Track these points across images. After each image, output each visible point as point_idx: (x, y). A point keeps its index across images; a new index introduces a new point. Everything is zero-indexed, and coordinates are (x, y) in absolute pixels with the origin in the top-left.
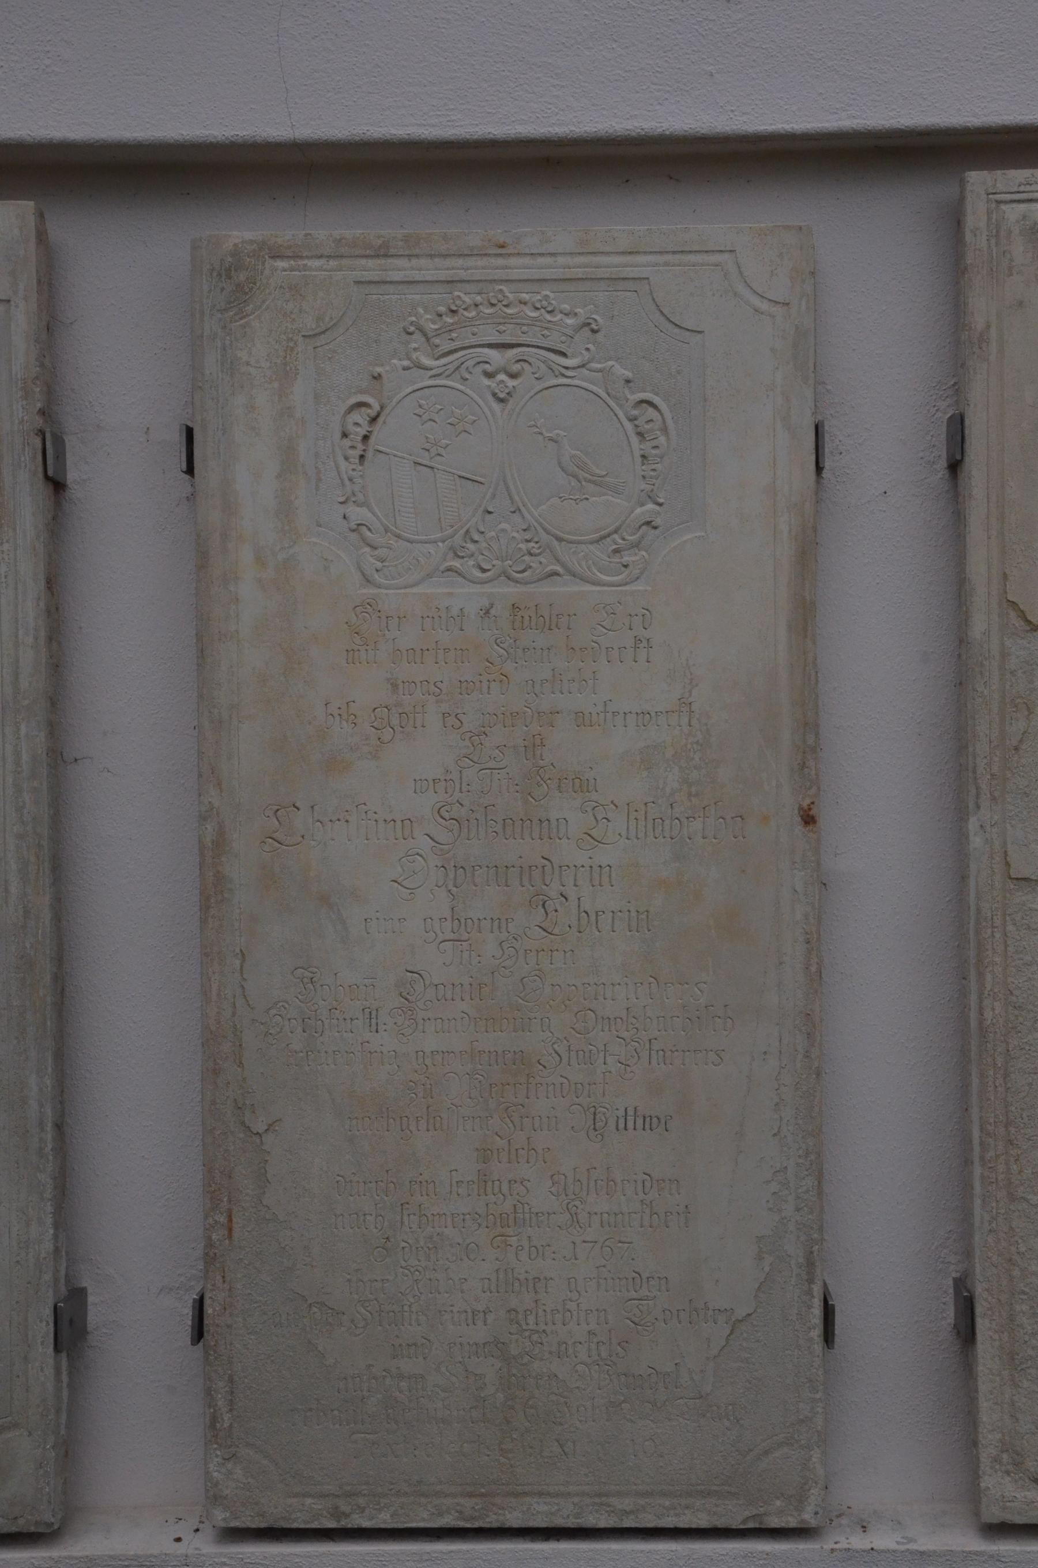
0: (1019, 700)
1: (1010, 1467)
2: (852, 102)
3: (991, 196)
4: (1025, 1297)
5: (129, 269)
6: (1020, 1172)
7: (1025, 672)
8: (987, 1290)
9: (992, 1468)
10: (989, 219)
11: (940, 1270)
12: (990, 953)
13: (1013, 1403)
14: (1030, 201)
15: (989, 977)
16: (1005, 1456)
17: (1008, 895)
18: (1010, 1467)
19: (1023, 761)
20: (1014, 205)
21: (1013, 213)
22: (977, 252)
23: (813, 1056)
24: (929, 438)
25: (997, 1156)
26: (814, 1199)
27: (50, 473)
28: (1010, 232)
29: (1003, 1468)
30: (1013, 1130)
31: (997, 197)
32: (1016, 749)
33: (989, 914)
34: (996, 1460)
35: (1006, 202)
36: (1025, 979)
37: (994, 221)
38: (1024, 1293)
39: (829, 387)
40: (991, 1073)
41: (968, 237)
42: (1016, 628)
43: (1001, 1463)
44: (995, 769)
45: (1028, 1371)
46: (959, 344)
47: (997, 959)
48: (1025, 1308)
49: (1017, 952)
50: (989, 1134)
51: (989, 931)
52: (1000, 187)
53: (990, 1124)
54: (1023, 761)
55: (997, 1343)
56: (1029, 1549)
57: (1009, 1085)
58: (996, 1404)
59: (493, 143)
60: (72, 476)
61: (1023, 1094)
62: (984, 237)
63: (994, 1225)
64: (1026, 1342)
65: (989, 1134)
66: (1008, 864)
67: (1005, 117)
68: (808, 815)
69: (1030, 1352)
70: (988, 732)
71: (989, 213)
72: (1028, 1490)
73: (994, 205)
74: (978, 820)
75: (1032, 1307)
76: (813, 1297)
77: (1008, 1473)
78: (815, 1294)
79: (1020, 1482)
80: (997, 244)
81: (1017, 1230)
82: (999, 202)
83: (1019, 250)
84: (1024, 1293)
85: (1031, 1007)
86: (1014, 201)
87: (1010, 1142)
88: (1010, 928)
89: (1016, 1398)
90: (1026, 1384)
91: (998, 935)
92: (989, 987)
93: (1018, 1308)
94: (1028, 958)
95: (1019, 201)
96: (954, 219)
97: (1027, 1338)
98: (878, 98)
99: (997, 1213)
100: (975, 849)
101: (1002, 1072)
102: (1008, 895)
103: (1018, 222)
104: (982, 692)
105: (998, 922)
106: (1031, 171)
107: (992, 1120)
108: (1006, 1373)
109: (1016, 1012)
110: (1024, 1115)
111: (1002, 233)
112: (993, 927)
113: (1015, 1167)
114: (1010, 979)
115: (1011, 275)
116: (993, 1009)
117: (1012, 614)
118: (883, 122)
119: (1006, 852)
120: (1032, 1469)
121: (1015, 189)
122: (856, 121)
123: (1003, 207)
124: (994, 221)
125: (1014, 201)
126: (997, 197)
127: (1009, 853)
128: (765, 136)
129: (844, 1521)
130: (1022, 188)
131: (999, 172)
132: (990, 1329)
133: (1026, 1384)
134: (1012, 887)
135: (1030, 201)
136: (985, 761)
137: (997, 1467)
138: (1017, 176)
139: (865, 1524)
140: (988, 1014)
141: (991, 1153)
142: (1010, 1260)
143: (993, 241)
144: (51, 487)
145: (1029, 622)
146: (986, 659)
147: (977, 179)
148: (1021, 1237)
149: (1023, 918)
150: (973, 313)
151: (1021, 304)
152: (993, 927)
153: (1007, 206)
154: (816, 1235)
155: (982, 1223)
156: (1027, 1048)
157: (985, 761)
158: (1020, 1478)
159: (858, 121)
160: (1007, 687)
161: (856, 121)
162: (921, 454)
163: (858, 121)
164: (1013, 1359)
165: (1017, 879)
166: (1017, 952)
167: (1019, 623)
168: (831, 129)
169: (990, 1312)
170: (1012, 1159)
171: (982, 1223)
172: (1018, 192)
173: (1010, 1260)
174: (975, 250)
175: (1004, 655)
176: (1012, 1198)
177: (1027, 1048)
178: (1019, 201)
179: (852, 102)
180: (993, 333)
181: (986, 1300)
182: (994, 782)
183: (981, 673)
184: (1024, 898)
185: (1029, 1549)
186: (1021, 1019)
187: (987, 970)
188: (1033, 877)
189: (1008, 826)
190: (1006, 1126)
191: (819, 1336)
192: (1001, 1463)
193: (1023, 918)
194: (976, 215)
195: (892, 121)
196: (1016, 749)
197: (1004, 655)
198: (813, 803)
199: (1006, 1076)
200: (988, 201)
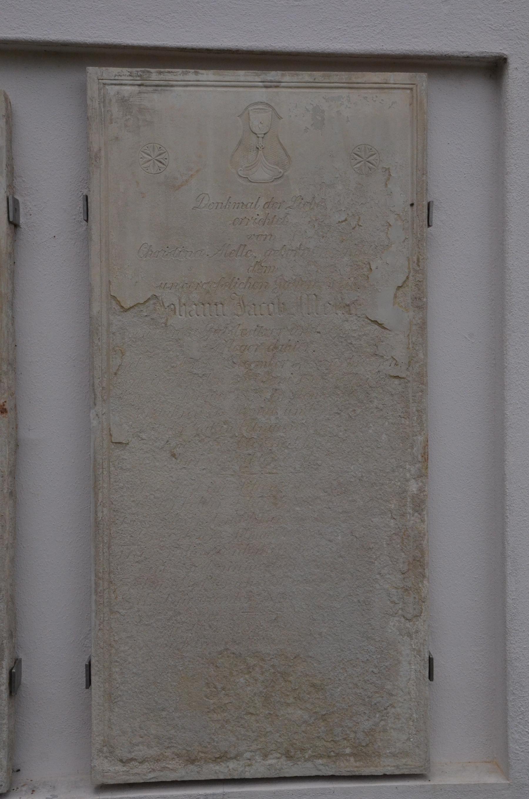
0: (117, 348)
1: (108, 755)
2: (23, 24)
3: (100, 81)
4: (117, 664)
5: (40, 106)
6: (116, 598)
7: (120, 334)
8: (97, 661)
9: (98, 755)
10: (100, 93)
11: (84, 651)
12: (101, 482)
13: (110, 720)
14: (121, 84)
15: (100, 495)
16: (105, 749)
17: (111, 451)
18: (108, 755)
19: (119, 380)
20: (113, 86)
21: (112, 90)
22: (93, 110)
23: (5, 538)
24: (78, 208)
25: (104, 590)
26: (4, 615)
27: (11, 220)
28: (111, 100)
29: (104, 755)
30: (112, 576)
31: (104, 81)
32: (115, 374)
33: (101, 461)
34: (101, 751)
35: (108, 85)
36: (119, 495)
37: (102, 94)
38: (117, 662)
39: (24, 179)
40: (101, 545)
41: (89, 102)
42: (116, 310)
43: (102, 752)
44: (104, 385)
45: (118, 703)
46: (90, 159)
47: (105, 485)
48: (117, 670)
49: (115, 482)
50: (100, 578)
51: (101, 470)
52: (105, 76)
53: (100, 573)
54: (119, 380)
55: (102, 689)
56: (115, 797)
57: (111, 552)
58: (101, 721)
59: (133, 47)
60: (22, 220)
61: (119, 557)
62: (97, 102)
63: (101, 626)
64: (118, 688)
65: (100, 578)
66: (111, 435)
67: (106, 39)
68: (3, 408)
69: (120, 693)
70: (100, 365)
71: (99, 90)
72: (117, 766)
73: (102, 86)
74: (95, 411)
75: (121, 669)
76: (3, 668)
77: (106, 757)
78: (4, 666)
79: (113, 762)
80: (104, 107)
81: (114, 629)
82: (104, 84)
83: (115, 110)
84: (117, 662)
85: (122, 511)
86: (112, 84)
87: (111, 582)
88: (112, 469)
89: (111, 718)
90: (117, 710)
91: (105, 473)
92: (100, 500)
93: (114, 670)
94: (122, 485)
95: (115, 84)
96: (83, 90)
97: (118, 685)
98: (38, 24)
99: (104, 620)
100: (93, 427)
101: (107, 545)
102: (111, 451)
103: (115, 95)
104: (97, 344)
105: (105, 466)
106: (121, 69)
107: (101, 571)
108: (106, 705)
109: (115, 513)
110: (118, 568)
111: (107, 101)
112: (103, 468)
113: (113, 595)
114: (112, 496)
115: (112, 123)
116: (103, 512)
117: (114, 303)
118: (41, 37)
119: (110, 429)
120: (119, 755)
121: (113, 78)
122: (25, 35)
123: (107, 87)
124: (102, 94)
125: (112, 84)
126: (104, 81)
127: (111, 429)
128: (125, 46)
129: (24, 788)
130: (116, 78)
131: (104, 68)
132: (98, 682)
133: (117, 710)
134: (113, 447)
135: (121, 84)
136: (99, 380)
137: (101, 755)
138: (114, 71)
139: (35, 789)
140: (100, 515)
141: (101, 588)
142: (110, 645)
143: (102, 105)
144: (13, 226)
145: (122, 307)
146: (99, 326)
147: (93, 71)
148: (116, 632)
149: (119, 464)
150: (91, 142)
151: (117, 138)
152: (103, 468)
153: (110, 86)
154: (5, 635)
155: (95, 625)
156: (120, 532)
157: (99, 380)
158: (113, 760)
159: (27, 35)
160: (111, 341)
161: (25, 35)
162: (74, 217)
163: (27, 35)
164: (111, 697)
165: (116, 443)
166: (115, 482)
167: (117, 308)
168: (72, 41)
169: (98, 673)
170: (112, 592)
171: (95, 625)
172: (115, 80)
173: (110, 645)
174: (92, 108)
175: (110, 324)
176: (112, 612)
177: (120, 532)
178: (115, 84)
179: (23, 24)
180: (103, 153)
181: (97, 666)
182: (104, 391)
183: (97, 334)
184: (119, 453)
185: (115, 797)
186: (117, 517)
187: (100, 491)
188: (124, 442)
189: (111, 415)
190: (109, 574)
191: (6, 689)
192: (102, 752)
193: (119, 464)
194: (93, 89)
195: (45, 37)
196: (115, 374)
197: (110, 324)
198: (5, 402)
199: (109, 548)
200: (99, 83)
